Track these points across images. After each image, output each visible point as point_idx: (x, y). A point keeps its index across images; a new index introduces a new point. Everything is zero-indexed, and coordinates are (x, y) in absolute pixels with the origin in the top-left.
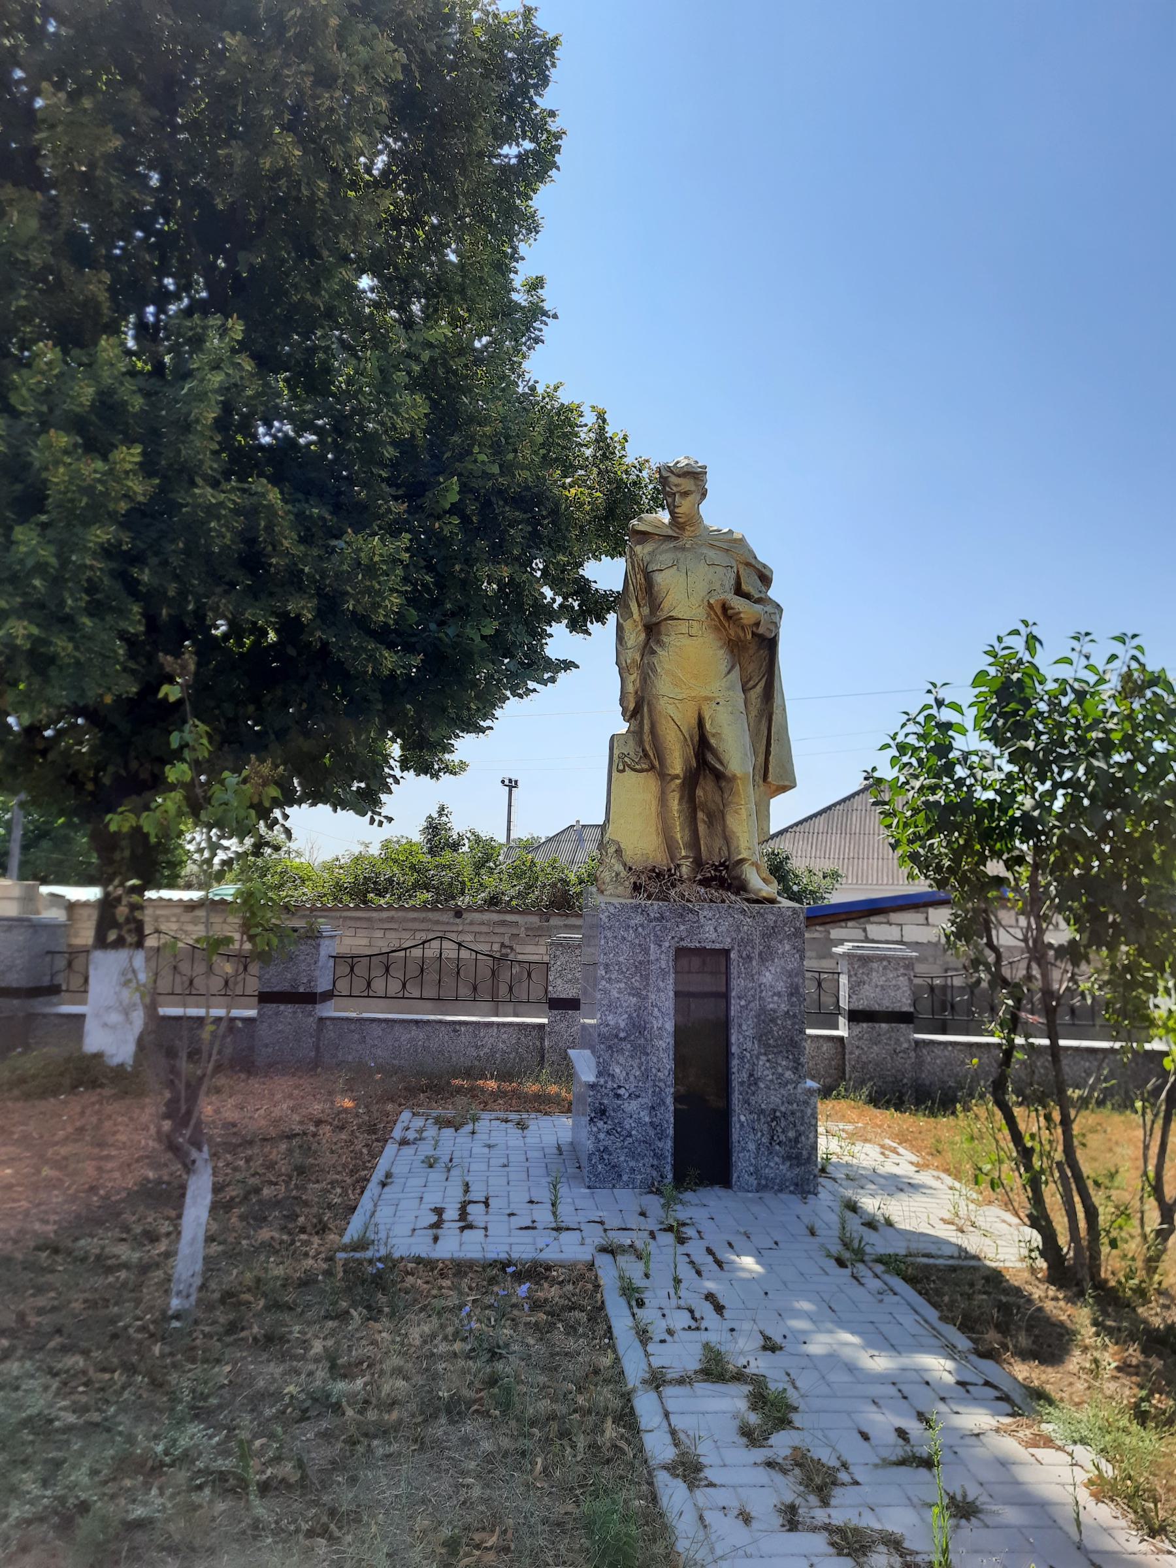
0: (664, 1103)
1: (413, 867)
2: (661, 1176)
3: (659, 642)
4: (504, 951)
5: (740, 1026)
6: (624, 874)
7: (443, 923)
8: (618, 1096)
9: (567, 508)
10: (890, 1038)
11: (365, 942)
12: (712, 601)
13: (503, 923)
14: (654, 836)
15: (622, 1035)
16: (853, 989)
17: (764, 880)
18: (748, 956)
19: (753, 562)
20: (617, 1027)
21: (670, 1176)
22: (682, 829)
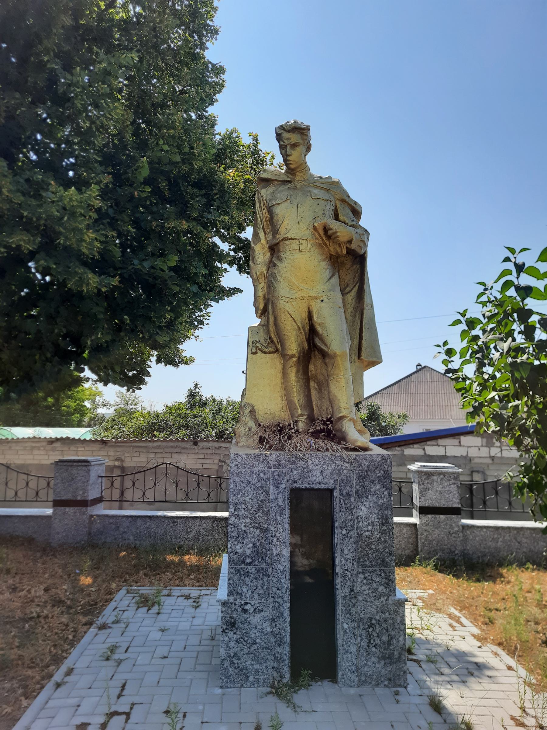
0: (282, 615)
1: (179, 416)
2: (281, 677)
3: (279, 258)
4: (220, 464)
5: (342, 550)
6: (254, 429)
7: (187, 449)
8: (245, 611)
9: (229, 188)
10: (446, 524)
11: (144, 460)
12: (316, 224)
13: (220, 448)
14: (279, 401)
15: (248, 561)
16: (422, 493)
17: (360, 432)
18: (348, 494)
19: (347, 199)
20: (244, 554)
21: (288, 676)
22: (299, 394)
